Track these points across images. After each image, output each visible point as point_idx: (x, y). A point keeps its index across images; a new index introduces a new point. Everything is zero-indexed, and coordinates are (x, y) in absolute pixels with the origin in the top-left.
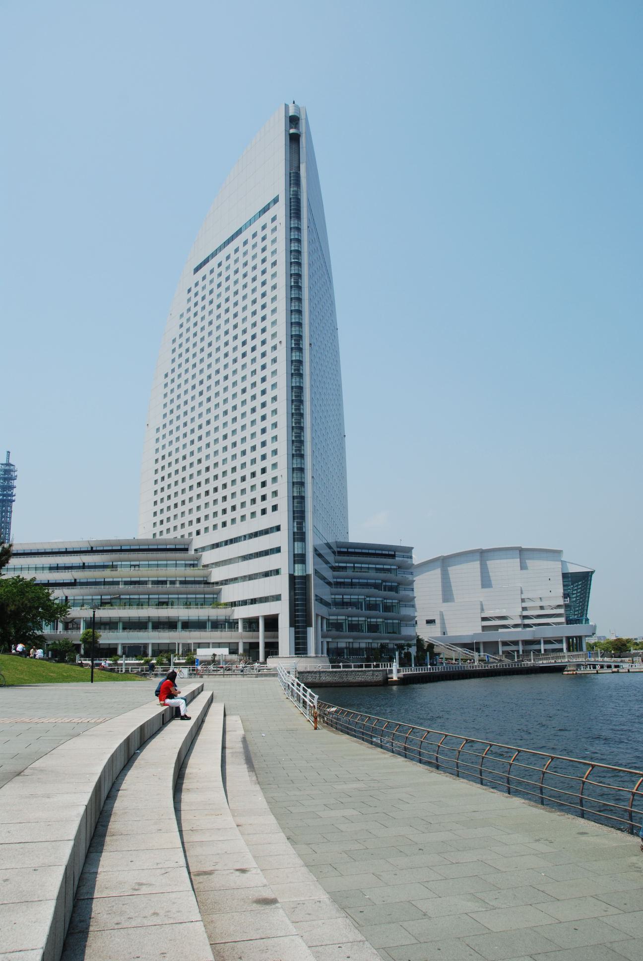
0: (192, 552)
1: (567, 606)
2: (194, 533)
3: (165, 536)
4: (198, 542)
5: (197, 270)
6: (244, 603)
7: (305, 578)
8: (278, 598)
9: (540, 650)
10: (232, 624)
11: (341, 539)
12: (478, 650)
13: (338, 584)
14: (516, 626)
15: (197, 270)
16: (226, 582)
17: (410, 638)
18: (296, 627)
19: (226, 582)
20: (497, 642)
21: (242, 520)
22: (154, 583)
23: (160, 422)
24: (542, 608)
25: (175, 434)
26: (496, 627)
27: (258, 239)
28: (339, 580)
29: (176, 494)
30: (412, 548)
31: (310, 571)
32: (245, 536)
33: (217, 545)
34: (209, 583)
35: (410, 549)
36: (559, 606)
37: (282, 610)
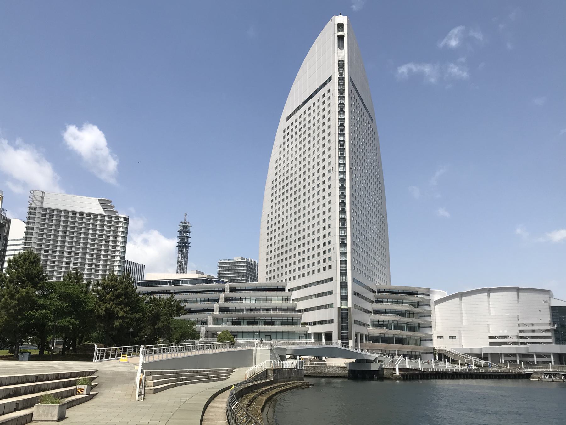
0: (287, 291)
1: (555, 331)
2: (288, 279)
6: (314, 323)
8: (331, 321)
10: (306, 335)
14: (514, 343)
15: (288, 118)
18: (342, 340)
22: (264, 310)
23: (269, 210)
26: (500, 344)
29: (309, 235)
31: (350, 305)
33: (299, 288)
34: (295, 311)
36: (547, 331)
37: (334, 328)
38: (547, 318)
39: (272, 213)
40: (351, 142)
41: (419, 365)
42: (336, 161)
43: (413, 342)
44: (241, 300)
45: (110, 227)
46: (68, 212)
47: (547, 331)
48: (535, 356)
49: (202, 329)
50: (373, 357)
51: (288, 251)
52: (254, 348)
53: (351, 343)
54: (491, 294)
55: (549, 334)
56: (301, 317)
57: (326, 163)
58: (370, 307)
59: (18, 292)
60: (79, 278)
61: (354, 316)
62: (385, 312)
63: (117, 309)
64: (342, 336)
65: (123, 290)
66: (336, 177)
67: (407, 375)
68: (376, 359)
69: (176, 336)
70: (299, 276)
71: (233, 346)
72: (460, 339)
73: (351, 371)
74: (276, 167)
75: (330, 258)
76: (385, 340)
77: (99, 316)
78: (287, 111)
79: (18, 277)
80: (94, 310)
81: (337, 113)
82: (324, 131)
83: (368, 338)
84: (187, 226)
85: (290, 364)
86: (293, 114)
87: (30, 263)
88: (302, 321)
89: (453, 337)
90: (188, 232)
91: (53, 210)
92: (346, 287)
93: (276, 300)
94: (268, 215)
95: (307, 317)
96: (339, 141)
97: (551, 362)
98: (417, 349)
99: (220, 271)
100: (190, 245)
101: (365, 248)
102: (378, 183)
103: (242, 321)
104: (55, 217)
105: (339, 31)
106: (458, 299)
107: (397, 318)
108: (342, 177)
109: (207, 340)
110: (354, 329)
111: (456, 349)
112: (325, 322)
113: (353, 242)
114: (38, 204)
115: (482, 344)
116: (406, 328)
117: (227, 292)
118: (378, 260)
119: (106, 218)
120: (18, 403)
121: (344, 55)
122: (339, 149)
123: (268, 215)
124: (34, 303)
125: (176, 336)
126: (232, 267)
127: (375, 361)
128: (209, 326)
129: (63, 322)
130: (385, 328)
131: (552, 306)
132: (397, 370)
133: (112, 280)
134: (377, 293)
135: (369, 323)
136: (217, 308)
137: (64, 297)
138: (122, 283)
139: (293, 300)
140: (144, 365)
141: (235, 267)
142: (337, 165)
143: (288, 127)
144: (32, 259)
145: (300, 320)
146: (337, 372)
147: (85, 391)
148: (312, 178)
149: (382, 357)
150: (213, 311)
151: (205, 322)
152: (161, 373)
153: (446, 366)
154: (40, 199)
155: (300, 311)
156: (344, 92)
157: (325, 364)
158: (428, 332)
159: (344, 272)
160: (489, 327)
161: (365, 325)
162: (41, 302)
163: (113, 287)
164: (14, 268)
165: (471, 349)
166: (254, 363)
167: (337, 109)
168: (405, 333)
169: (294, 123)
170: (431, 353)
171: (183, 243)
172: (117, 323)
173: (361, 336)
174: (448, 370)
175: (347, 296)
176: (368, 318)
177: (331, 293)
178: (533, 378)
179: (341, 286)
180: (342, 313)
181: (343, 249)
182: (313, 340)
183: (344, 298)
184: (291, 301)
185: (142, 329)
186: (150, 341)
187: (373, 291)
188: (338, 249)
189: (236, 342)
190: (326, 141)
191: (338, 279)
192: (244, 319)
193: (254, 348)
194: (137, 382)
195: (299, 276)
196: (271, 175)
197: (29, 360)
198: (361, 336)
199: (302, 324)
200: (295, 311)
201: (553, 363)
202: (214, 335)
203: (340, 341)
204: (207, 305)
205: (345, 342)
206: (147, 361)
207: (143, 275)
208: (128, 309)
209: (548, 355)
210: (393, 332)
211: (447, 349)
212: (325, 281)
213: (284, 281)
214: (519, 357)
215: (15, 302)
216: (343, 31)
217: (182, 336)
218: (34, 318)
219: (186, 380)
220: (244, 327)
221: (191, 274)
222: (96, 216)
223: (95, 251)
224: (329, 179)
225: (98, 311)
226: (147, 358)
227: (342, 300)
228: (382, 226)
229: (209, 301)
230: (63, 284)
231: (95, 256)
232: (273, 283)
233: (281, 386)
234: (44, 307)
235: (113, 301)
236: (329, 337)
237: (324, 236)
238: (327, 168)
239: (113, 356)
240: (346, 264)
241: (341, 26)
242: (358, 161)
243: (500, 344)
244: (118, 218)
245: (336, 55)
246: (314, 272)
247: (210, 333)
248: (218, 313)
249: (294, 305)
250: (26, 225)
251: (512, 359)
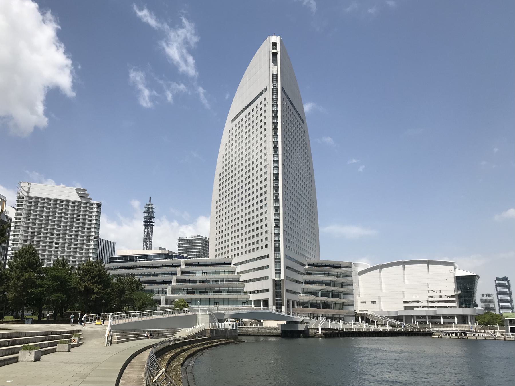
0: (232, 265)
2: (233, 256)
4: (234, 261)
6: (254, 292)
8: (268, 290)
9: (440, 322)
10: (248, 302)
15: (233, 120)
16: (247, 281)
18: (276, 306)
19: (247, 281)
22: (213, 281)
23: (218, 198)
24: (441, 297)
25: (252, 196)
26: (412, 308)
31: (283, 277)
33: (242, 263)
34: (239, 282)
36: (452, 296)
37: (269, 296)
38: (452, 285)
40: (283, 142)
41: (340, 326)
42: (270, 158)
43: (338, 307)
44: (194, 273)
45: (86, 212)
46: (50, 200)
47: (452, 296)
48: (442, 318)
49: (163, 297)
50: (300, 319)
51: (230, 234)
52: (197, 313)
53: (283, 308)
54: (406, 266)
55: (454, 299)
56: (244, 287)
57: (263, 160)
58: (300, 278)
59: (23, 276)
60: (64, 263)
61: (285, 287)
62: (314, 282)
63: (93, 286)
64: (276, 303)
65: (97, 272)
66: (270, 171)
67: (328, 334)
68: (303, 321)
69: (138, 305)
70: (253, 249)
71: (188, 311)
72: (380, 304)
73: (282, 331)
74: (223, 162)
75: (266, 239)
76: (314, 305)
77: (80, 292)
78: (232, 114)
79: (22, 265)
80: (76, 288)
81: (271, 118)
82: (261, 133)
83: (299, 304)
84: (152, 208)
85: (228, 325)
86: (236, 117)
87: (30, 254)
88: (245, 291)
89: (374, 302)
90: (152, 213)
91: (37, 198)
92: (280, 262)
93: (224, 274)
94: (217, 202)
95: (248, 287)
96: (273, 142)
97: (455, 323)
98: (342, 313)
99: (179, 247)
100: (154, 224)
101: (296, 229)
102: (308, 174)
103: (195, 291)
104: (39, 204)
105: (273, 49)
106: (378, 270)
107: (324, 287)
108: (276, 171)
109: (167, 306)
110: (286, 296)
111: (376, 312)
113: (285, 225)
114: (26, 194)
115: (398, 308)
116: (331, 295)
117: (183, 266)
118: (308, 239)
119: (82, 204)
120: (48, 344)
121: (277, 69)
122: (273, 148)
123: (217, 202)
124: (34, 283)
125: (138, 305)
126: (189, 243)
127: (302, 322)
128: (168, 295)
129: (54, 296)
130: (313, 296)
131: (457, 275)
132: (320, 330)
133: (89, 265)
134: (307, 267)
135: (300, 292)
137: (54, 278)
138: (96, 267)
139: (237, 273)
140: (111, 326)
141: (192, 243)
142: (272, 162)
143: (233, 128)
144: (31, 251)
145: (243, 289)
146: (272, 332)
147: (77, 341)
148: (252, 172)
149: (308, 320)
150: (171, 282)
151: (165, 292)
152: (124, 332)
153: (363, 326)
154: (27, 190)
155: (243, 282)
156: (277, 100)
157: (262, 325)
158: (350, 298)
159: (277, 250)
160: (403, 294)
161: (296, 293)
162: (38, 282)
163: (90, 270)
164: (19, 258)
165: (388, 312)
166: (197, 323)
167: (272, 115)
168: (331, 300)
169: (241, 122)
170: (353, 316)
171: (148, 222)
172: (93, 297)
173: (293, 303)
174: (354, 329)
175: (280, 270)
176: (299, 288)
177: (267, 267)
178: (435, 335)
179: (275, 262)
180: (276, 284)
181: (277, 232)
182: (253, 306)
184: (236, 274)
185: (111, 300)
186: (118, 309)
187: (304, 265)
188: (273, 231)
189: (190, 309)
190: (263, 141)
191: (273, 256)
192: (197, 289)
193: (197, 313)
194: (106, 336)
195: (253, 249)
196: (219, 169)
197: (32, 323)
198: (293, 303)
199: (244, 293)
200: (239, 282)
201: (456, 323)
202: (172, 302)
203: (274, 307)
204: (167, 278)
205: (279, 308)
206: (114, 323)
207: (114, 251)
208: (101, 286)
209: (453, 317)
210: (320, 299)
211: (368, 313)
212: (263, 257)
213: (230, 257)
215: (21, 283)
216: (276, 49)
217: (143, 304)
218: (34, 294)
219: (141, 336)
220: (197, 296)
221: (154, 251)
222: (74, 202)
223: (74, 233)
224: (265, 173)
225: (80, 288)
226: (114, 322)
227: (276, 273)
228: (312, 210)
229: (168, 274)
230: (54, 269)
231: (73, 237)
232: (221, 258)
233: (216, 342)
234: (41, 286)
235: (90, 280)
236: (266, 303)
237: (261, 221)
238: (264, 164)
239: (91, 321)
240: (279, 244)
241: (274, 45)
242: (289, 157)
243: (412, 308)
244: (92, 204)
246: (262, 247)
247: (169, 301)
248: (175, 284)
249: (238, 277)
250: (16, 212)
251: (423, 320)
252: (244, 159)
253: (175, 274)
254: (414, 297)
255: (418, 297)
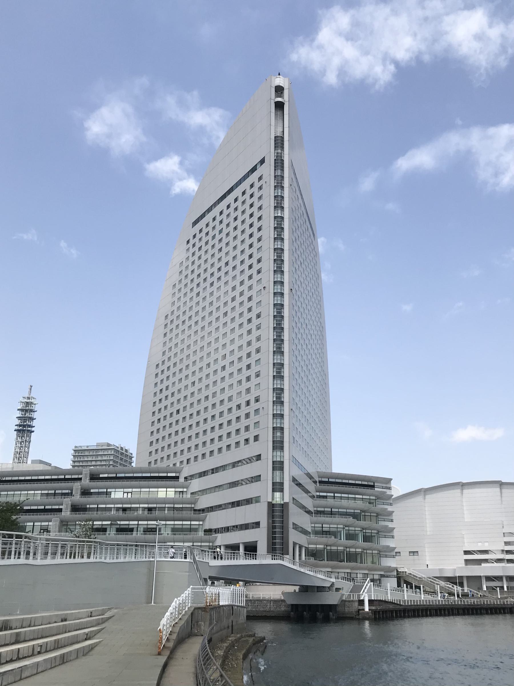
2: (185, 462)
3: (159, 465)
5: (195, 223)
6: (227, 529)
7: (284, 507)
11: (323, 469)
12: (461, 585)
13: (318, 513)
15: (195, 223)
16: (211, 509)
17: (390, 569)
19: (211, 509)
20: (480, 577)
21: (236, 447)
26: (479, 562)
27: (247, 196)
28: (319, 509)
30: (391, 479)
32: (213, 470)
33: (203, 474)
35: (388, 481)
37: (260, 536)
39: (163, 362)
68: (333, 584)
90: (32, 411)
95: (214, 520)
100: (33, 429)
105: (277, 96)
112: (245, 527)
115: (455, 565)
130: (333, 537)
136: (77, 489)
142: (272, 284)
146: (267, 609)
171: (24, 426)
177: (257, 478)
183: (278, 487)
188: (270, 409)
214: (507, 581)
221: (28, 466)
236: (251, 549)
240: (283, 433)
241: (279, 90)
243: (479, 562)
245: (273, 128)
252: (194, 319)
253: (71, 494)
254: (480, 544)
255: (486, 544)
